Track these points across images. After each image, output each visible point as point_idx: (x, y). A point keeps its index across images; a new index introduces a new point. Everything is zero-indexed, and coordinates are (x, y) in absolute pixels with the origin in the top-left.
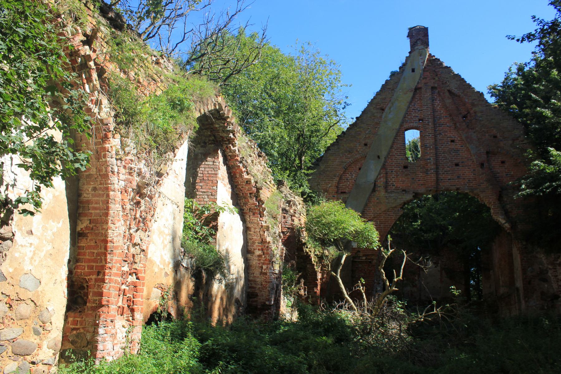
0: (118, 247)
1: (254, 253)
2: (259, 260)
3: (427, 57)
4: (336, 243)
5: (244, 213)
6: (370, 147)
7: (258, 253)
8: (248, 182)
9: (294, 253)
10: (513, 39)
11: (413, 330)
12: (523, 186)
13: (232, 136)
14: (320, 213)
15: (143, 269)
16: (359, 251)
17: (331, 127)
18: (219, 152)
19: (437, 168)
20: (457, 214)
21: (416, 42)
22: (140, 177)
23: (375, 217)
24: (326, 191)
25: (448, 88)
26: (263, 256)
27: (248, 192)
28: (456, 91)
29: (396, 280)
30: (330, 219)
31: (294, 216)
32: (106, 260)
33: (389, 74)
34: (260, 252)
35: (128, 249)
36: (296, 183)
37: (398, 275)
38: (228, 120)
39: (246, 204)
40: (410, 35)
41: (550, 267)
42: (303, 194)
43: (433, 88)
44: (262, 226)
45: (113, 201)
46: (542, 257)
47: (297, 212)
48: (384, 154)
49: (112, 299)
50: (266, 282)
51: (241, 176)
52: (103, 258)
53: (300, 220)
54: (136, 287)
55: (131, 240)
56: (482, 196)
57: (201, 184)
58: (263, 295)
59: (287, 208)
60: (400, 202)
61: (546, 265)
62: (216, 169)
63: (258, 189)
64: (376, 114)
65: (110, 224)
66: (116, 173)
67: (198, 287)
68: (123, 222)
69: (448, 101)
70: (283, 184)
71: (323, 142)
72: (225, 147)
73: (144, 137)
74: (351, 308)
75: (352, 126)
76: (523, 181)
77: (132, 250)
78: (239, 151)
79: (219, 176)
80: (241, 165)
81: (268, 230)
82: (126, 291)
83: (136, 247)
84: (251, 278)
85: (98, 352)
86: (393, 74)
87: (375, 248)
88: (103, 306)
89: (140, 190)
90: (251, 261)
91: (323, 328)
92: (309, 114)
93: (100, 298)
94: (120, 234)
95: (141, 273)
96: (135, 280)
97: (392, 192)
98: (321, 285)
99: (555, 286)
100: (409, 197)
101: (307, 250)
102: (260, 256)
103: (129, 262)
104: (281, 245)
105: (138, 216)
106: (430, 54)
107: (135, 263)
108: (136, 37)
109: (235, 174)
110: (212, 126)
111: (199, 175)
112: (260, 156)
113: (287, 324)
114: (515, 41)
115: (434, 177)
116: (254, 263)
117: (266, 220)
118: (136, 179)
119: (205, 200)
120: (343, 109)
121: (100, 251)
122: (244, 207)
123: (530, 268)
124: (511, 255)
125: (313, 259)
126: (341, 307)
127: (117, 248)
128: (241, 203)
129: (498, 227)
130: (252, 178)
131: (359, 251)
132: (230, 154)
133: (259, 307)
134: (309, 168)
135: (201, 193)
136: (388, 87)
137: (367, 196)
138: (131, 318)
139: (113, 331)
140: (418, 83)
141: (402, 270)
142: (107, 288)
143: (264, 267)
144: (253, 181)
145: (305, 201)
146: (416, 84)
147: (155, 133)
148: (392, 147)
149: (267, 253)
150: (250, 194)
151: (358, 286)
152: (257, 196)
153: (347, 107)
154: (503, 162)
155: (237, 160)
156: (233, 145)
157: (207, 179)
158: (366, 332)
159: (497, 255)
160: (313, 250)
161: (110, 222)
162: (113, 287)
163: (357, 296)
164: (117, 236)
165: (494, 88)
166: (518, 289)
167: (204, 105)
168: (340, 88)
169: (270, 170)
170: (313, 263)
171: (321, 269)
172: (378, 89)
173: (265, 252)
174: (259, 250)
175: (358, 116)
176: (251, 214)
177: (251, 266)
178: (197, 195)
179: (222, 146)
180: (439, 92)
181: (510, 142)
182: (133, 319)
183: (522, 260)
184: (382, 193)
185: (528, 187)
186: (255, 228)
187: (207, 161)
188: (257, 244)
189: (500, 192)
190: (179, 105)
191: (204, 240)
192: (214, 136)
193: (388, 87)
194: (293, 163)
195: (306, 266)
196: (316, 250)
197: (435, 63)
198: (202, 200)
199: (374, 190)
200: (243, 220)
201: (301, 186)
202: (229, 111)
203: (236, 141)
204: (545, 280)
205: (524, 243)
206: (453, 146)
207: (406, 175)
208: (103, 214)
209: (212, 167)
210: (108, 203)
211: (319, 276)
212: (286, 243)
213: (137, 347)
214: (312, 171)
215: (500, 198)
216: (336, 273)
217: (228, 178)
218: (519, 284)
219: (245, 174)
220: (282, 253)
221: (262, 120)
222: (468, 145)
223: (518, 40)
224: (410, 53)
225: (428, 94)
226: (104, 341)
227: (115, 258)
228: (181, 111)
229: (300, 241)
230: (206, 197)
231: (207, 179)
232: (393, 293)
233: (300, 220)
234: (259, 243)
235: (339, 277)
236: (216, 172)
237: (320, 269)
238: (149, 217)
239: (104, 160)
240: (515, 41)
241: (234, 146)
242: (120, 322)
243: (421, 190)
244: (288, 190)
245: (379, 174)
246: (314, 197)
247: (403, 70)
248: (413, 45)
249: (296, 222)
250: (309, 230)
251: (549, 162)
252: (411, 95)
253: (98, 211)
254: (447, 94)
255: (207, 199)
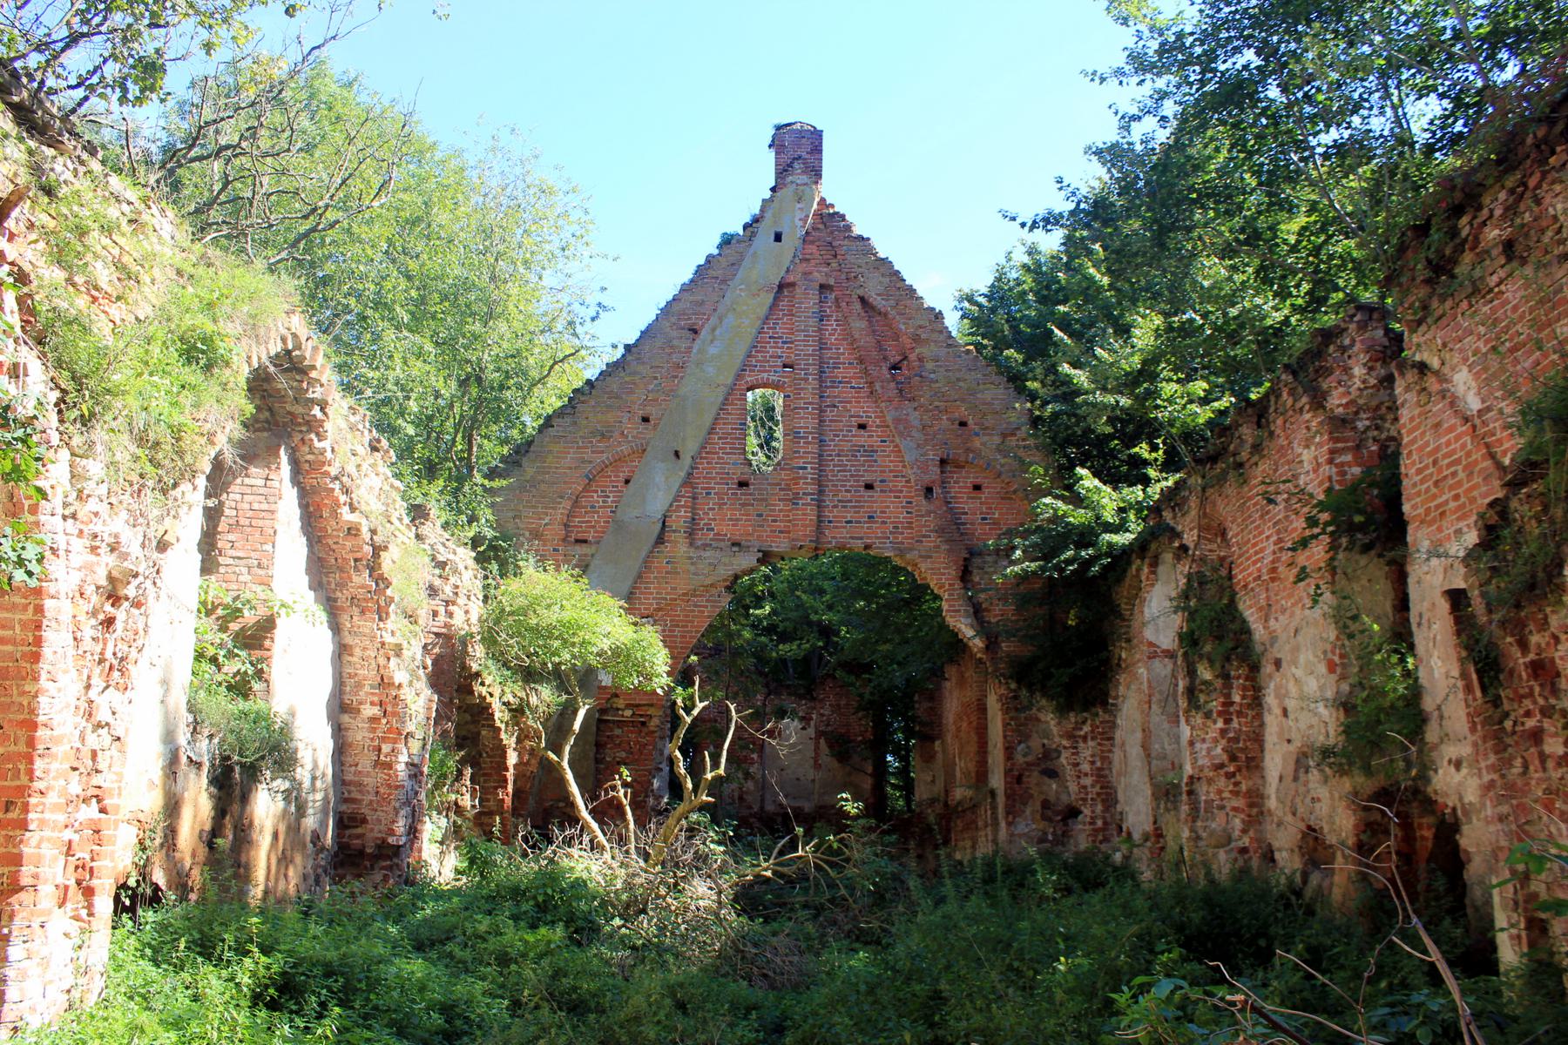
0: (62, 737)
1: (359, 711)
2: (373, 730)
3: (815, 206)
4: (558, 677)
5: (337, 608)
6: (655, 425)
7: (369, 711)
8: (353, 531)
9: (451, 700)
10: (1014, 219)
11: (749, 899)
12: (1018, 553)
13: (319, 415)
14: (522, 602)
15: (116, 785)
16: (617, 696)
17: (556, 363)
18: (282, 452)
19: (821, 492)
20: (889, 758)
21: (790, 165)
22: (115, 554)
23: (660, 609)
24: (536, 534)
25: (860, 292)
26: (384, 721)
27: (351, 557)
28: (878, 302)
29: (709, 776)
30: (551, 617)
31: (454, 603)
32: (30, 773)
33: (718, 240)
34: (375, 711)
35: (83, 739)
36: (460, 512)
37: (715, 765)
38: (314, 374)
39: (342, 585)
40: (777, 144)
41: (1065, 743)
42: (475, 542)
43: (823, 287)
44: (383, 644)
45: (53, 624)
46: (1049, 719)
47: (462, 591)
48: (690, 448)
49: (44, 871)
50: (389, 786)
51: (335, 514)
52: (22, 767)
53: (467, 612)
54: (97, 832)
55: (90, 715)
56: (923, 567)
57: (231, 537)
58: (379, 821)
59: (437, 582)
60: (725, 572)
61: (1057, 739)
62: (271, 499)
63: (377, 550)
64: (675, 342)
65: (44, 682)
66: (61, 553)
67: (220, 812)
68: (74, 673)
69: (859, 325)
70: (426, 516)
71: (533, 404)
72: (297, 438)
73: (125, 448)
74: (594, 846)
75: (613, 368)
76: (1017, 541)
77: (93, 741)
78: (333, 450)
79: (280, 515)
80: (336, 486)
81: (398, 655)
82: (74, 846)
83: (100, 731)
84: (349, 777)
85: (6, 1007)
86: (727, 241)
87: (659, 691)
88: (22, 889)
89: (114, 588)
90: (350, 733)
91: (532, 903)
92: (502, 326)
93: (13, 869)
94: (68, 706)
95: (111, 796)
96: (96, 815)
97: (705, 546)
98: (515, 782)
99: (1073, 787)
100: (747, 560)
101: (484, 691)
102: (374, 720)
103: (82, 770)
104: (422, 685)
105: (109, 655)
106: (823, 200)
107: (97, 771)
108: (85, 156)
109: (319, 507)
110: (266, 386)
111: (227, 512)
112: (374, 449)
113: (440, 895)
114: (1016, 224)
115: (811, 514)
116: (359, 738)
117: (394, 628)
118: (107, 561)
119: (241, 578)
120: (593, 319)
121: (13, 748)
122: (339, 594)
123: (1023, 745)
124: (982, 709)
125: (497, 715)
126: (569, 842)
127: (58, 740)
128: (329, 583)
129: (956, 646)
130: (364, 522)
131: (617, 696)
132: (310, 457)
133: (369, 851)
134: (492, 474)
135: (231, 561)
136: (712, 273)
137: (644, 554)
138: (84, 913)
139: (45, 951)
140: (788, 270)
141: (725, 753)
142: (34, 842)
143: (386, 748)
144: (365, 530)
145: (481, 559)
146: (782, 273)
147: (152, 437)
148: (712, 431)
149: (395, 714)
150: (356, 560)
151: (614, 788)
152: (374, 567)
153: (602, 315)
154: (977, 488)
155: (327, 474)
156: (318, 434)
157: (247, 522)
158: (634, 908)
159: (953, 703)
160: (497, 691)
161: (44, 676)
162: (49, 840)
163: (607, 813)
164: (61, 711)
165: (970, 299)
166: (993, 793)
167: (258, 343)
168: (587, 260)
169: (397, 483)
170: (498, 724)
171: (519, 741)
172: (687, 275)
173: (389, 709)
174: (372, 704)
175: (631, 342)
176: (356, 611)
177: (350, 745)
178: (219, 565)
179: (290, 436)
180: (837, 299)
181: (997, 440)
182: (91, 914)
183: (1005, 725)
184: (679, 547)
185: (1027, 556)
186: (365, 649)
187: (247, 476)
188: (367, 689)
189: (965, 559)
190: (203, 352)
191: (240, 688)
192: (270, 409)
193: (712, 273)
194: (449, 450)
195: (479, 733)
196: (507, 690)
197: (831, 223)
198: (234, 578)
199: (660, 540)
200: (336, 628)
201: (472, 519)
202: (315, 349)
203: (327, 426)
204: (1052, 774)
205: (1013, 686)
206: (863, 438)
207: (743, 505)
208: (24, 655)
209: (262, 491)
210: (39, 627)
211: (512, 758)
212: (437, 680)
213: (98, 983)
214: (504, 483)
215: (965, 575)
216: (559, 753)
217: (302, 518)
218: (997, 781)
219: (345, 509)
220: (429, 709)
221: (377, 338)
222: (897, 440)
223: (1023, 225)
224: (773, 190)
225: (808, 301)
226: (23, 977)
227: (55, 766)
228: (208, 368)
229: (464, 667)
230: (245, 570)
231: (247, 522)
232: (703, 808)
233: (468, 615)
234: (372, 687)
235: (565, 764)
236: (273, 507)
237: (514, 739)
238: (133, 654)
239: (31, 518)
240: (1016, 224)
241: (321, 438)
242: (61, 921)
243: (780, 545)
244: (440, 531)
245: (677, 498)
246: (506, 551)
247: (754, 234)
248: (783, 172)
249: (458, 620)
250: (490, 640)
251: (1078, 501)
252: (768, 299)
253: (9, 648)
254: (857, 306)
255: (245, 578)
